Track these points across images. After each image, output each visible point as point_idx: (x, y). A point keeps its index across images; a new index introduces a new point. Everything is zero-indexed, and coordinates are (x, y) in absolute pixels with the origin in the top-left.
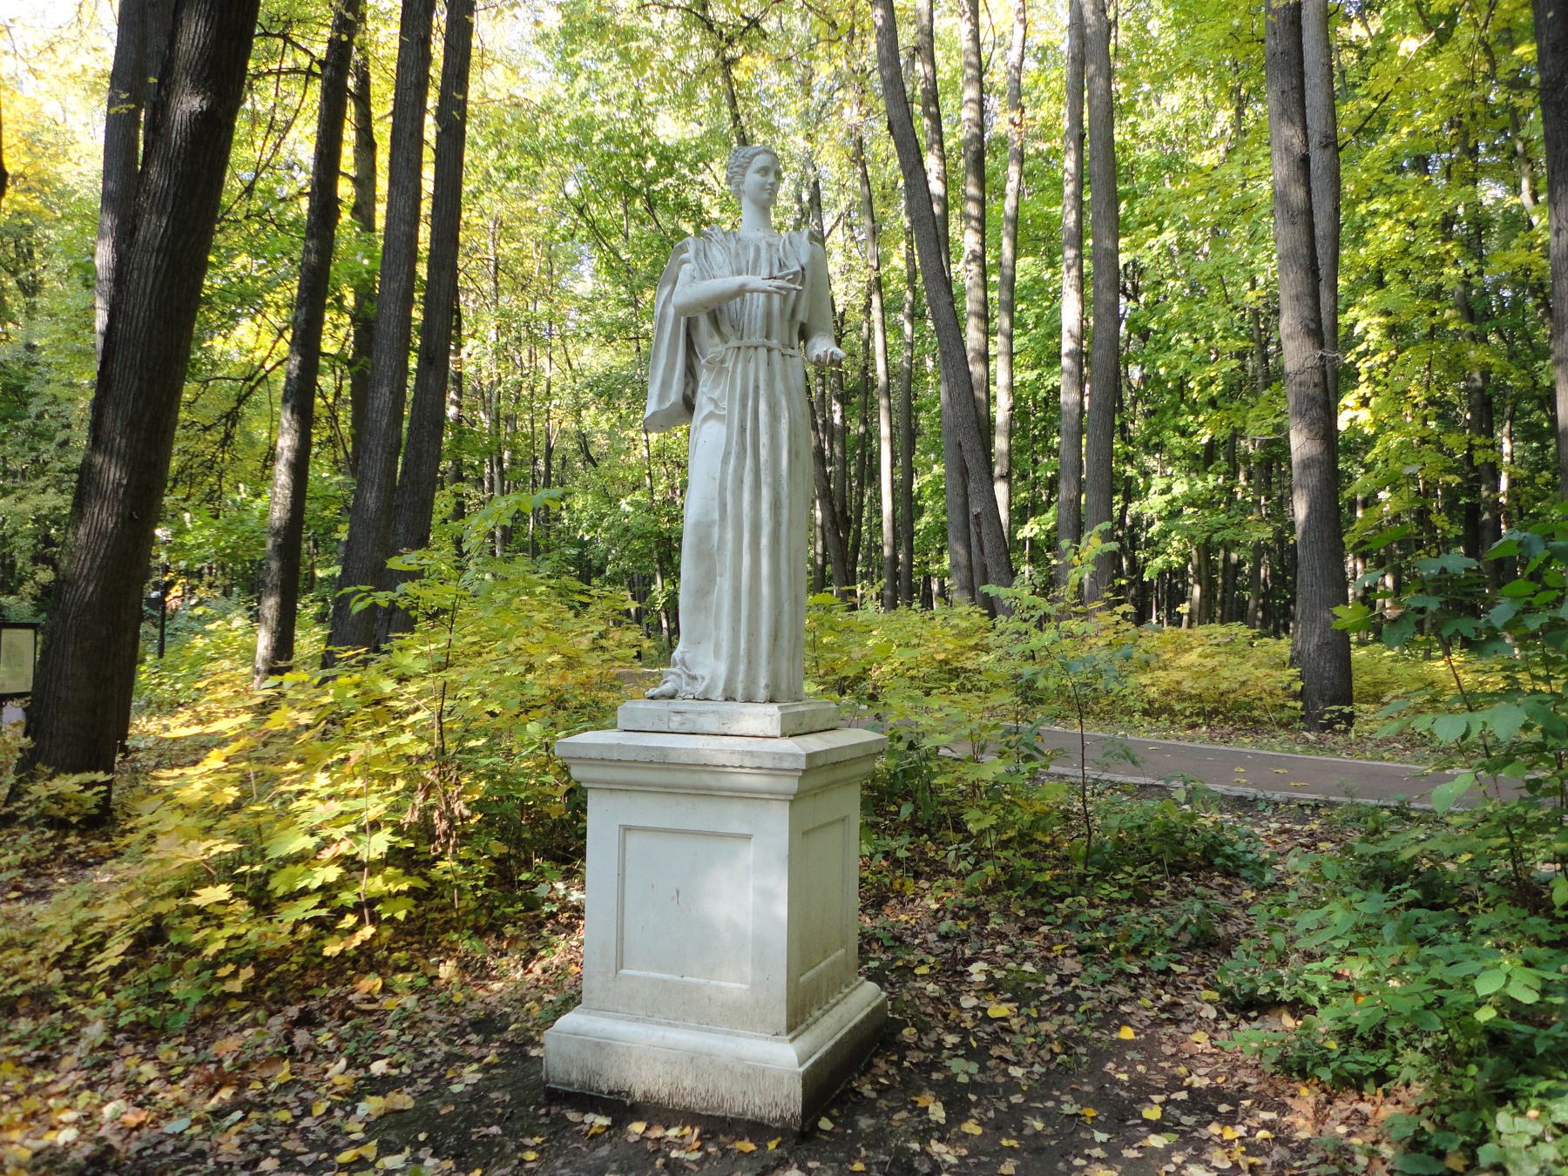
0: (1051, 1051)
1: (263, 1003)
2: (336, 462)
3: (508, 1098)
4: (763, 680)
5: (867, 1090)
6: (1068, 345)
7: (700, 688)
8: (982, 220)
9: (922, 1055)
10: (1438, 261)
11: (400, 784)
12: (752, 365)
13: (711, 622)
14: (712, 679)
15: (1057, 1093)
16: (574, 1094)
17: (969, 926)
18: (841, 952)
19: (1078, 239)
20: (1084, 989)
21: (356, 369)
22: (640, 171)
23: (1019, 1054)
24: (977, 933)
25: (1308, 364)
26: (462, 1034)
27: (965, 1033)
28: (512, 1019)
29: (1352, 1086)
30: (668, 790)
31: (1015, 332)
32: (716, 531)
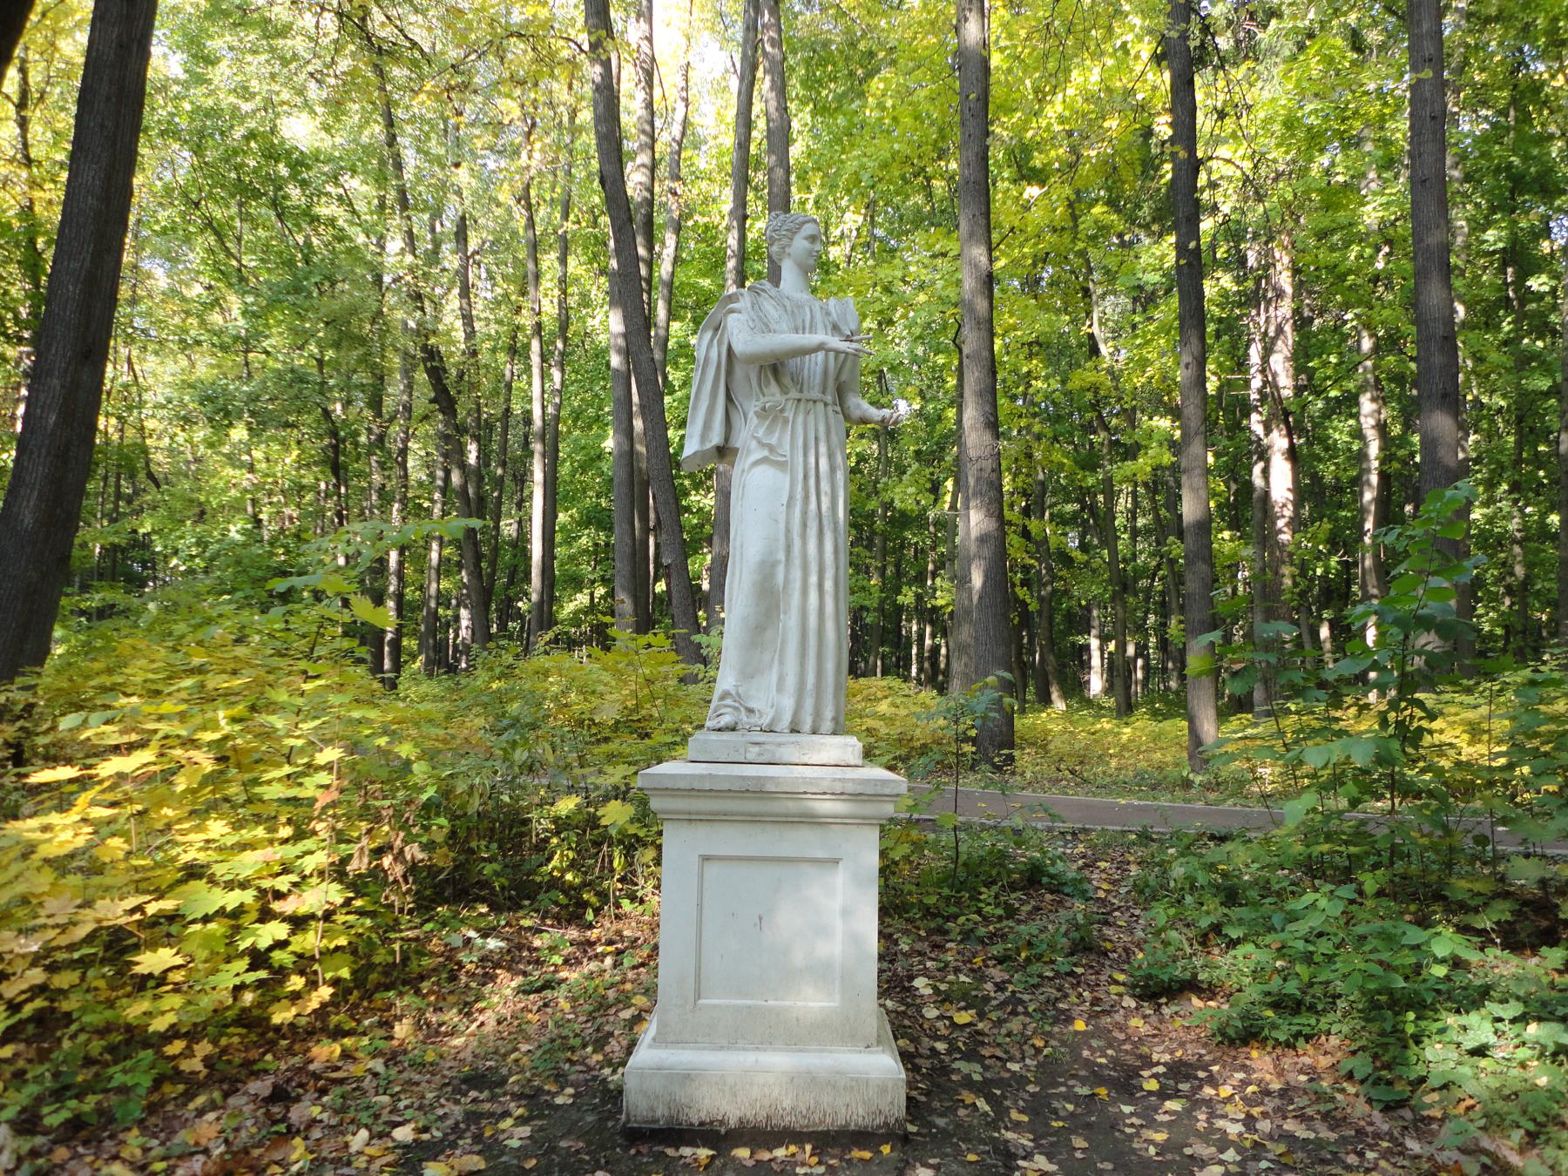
4: (829, 713)
7: (765, 721)
16: (661, 1130)
23: (1006, 1052)
30: (755, 819)
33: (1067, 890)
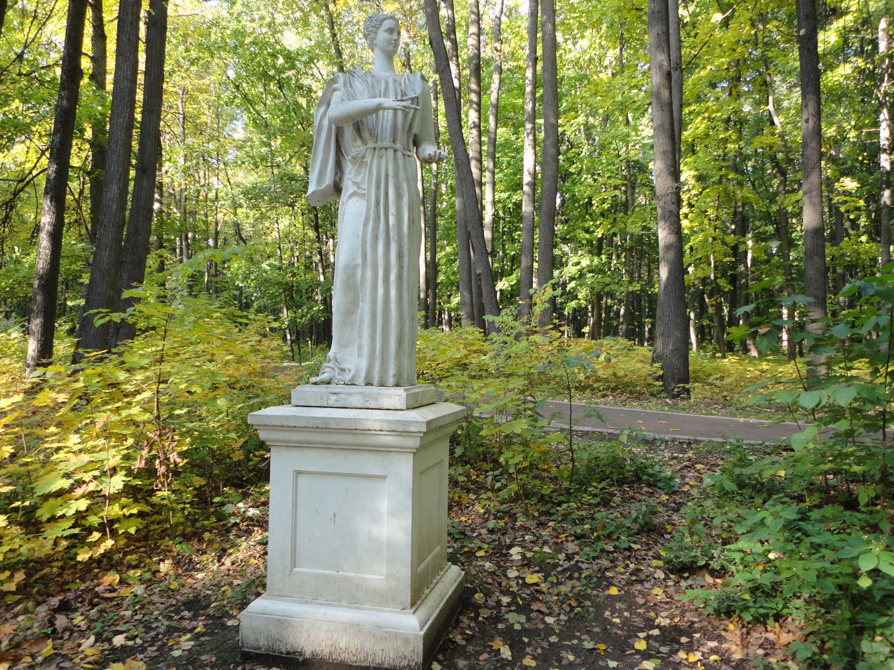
0: (570, 605)
1: (32, 595)
2: (81, 235)
3: (214, 659)
4: (392, 371)
5: (459, 639)
6: (527, 179)
7: (348, 377)
8: (479, 104)
9: (489, 612)
10: (726, 141)
11: (130, 441)
12: (384, 160)
13: (356, 333)
14: (356, 371)
15: (578, 634)
17: (506, 524)
18: (438, 548)
19: (533, 117)
20: (582, 562)
21: (93, 176)
22: (274, 67)
23: (550, 608)
24: (512, 528)
25: (670, 191)
26: (177, 612)
27: (513, 595)
28: (213, 599)
29: (759, 622)
30: (328, 447)
31: (497, 171)
32: (359, 271)
33: (660, 485)
